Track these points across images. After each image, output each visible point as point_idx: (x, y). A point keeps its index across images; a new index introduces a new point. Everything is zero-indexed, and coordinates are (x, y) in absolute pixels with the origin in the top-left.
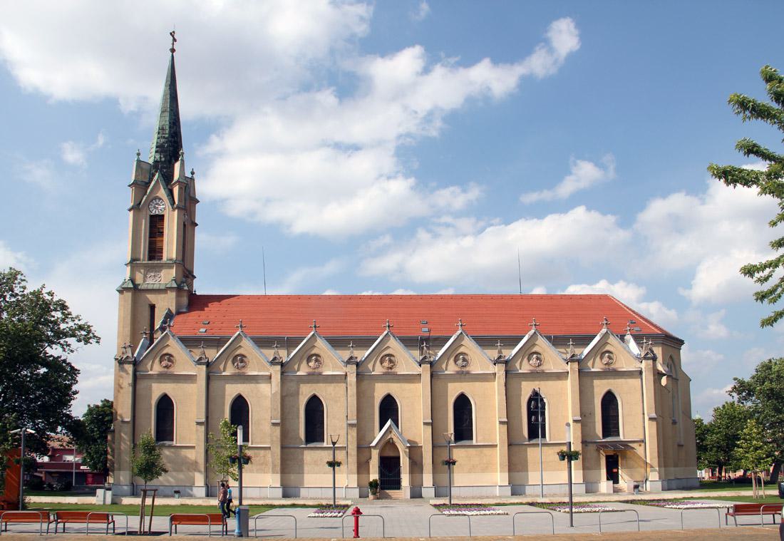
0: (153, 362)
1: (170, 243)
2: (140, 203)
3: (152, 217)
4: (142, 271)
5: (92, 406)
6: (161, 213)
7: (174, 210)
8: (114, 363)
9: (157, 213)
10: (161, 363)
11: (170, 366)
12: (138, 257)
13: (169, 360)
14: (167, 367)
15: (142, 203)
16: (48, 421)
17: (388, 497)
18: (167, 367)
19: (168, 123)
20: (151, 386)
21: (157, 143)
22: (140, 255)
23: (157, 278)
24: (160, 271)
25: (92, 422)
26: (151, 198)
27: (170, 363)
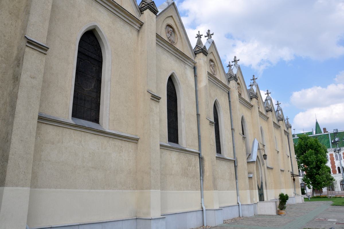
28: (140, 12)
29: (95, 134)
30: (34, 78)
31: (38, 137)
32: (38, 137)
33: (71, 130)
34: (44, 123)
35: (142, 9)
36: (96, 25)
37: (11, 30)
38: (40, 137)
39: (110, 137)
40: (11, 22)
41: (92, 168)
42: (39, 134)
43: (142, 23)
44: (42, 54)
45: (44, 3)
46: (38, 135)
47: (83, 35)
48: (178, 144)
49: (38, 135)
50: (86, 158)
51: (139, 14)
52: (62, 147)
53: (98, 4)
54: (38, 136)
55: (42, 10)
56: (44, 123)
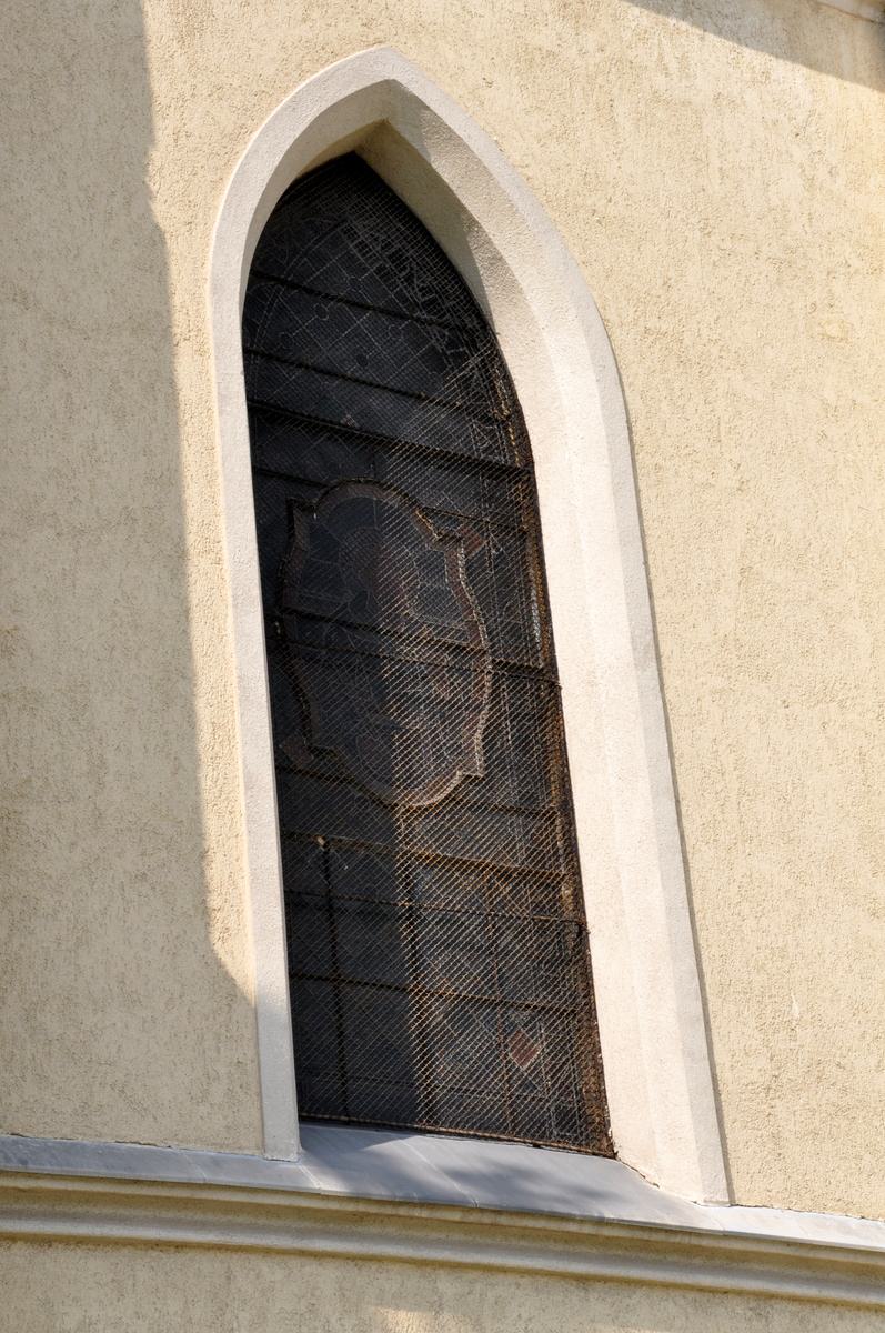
29: (583, 1280)
36: (390, 88)
39: (758, 1295)
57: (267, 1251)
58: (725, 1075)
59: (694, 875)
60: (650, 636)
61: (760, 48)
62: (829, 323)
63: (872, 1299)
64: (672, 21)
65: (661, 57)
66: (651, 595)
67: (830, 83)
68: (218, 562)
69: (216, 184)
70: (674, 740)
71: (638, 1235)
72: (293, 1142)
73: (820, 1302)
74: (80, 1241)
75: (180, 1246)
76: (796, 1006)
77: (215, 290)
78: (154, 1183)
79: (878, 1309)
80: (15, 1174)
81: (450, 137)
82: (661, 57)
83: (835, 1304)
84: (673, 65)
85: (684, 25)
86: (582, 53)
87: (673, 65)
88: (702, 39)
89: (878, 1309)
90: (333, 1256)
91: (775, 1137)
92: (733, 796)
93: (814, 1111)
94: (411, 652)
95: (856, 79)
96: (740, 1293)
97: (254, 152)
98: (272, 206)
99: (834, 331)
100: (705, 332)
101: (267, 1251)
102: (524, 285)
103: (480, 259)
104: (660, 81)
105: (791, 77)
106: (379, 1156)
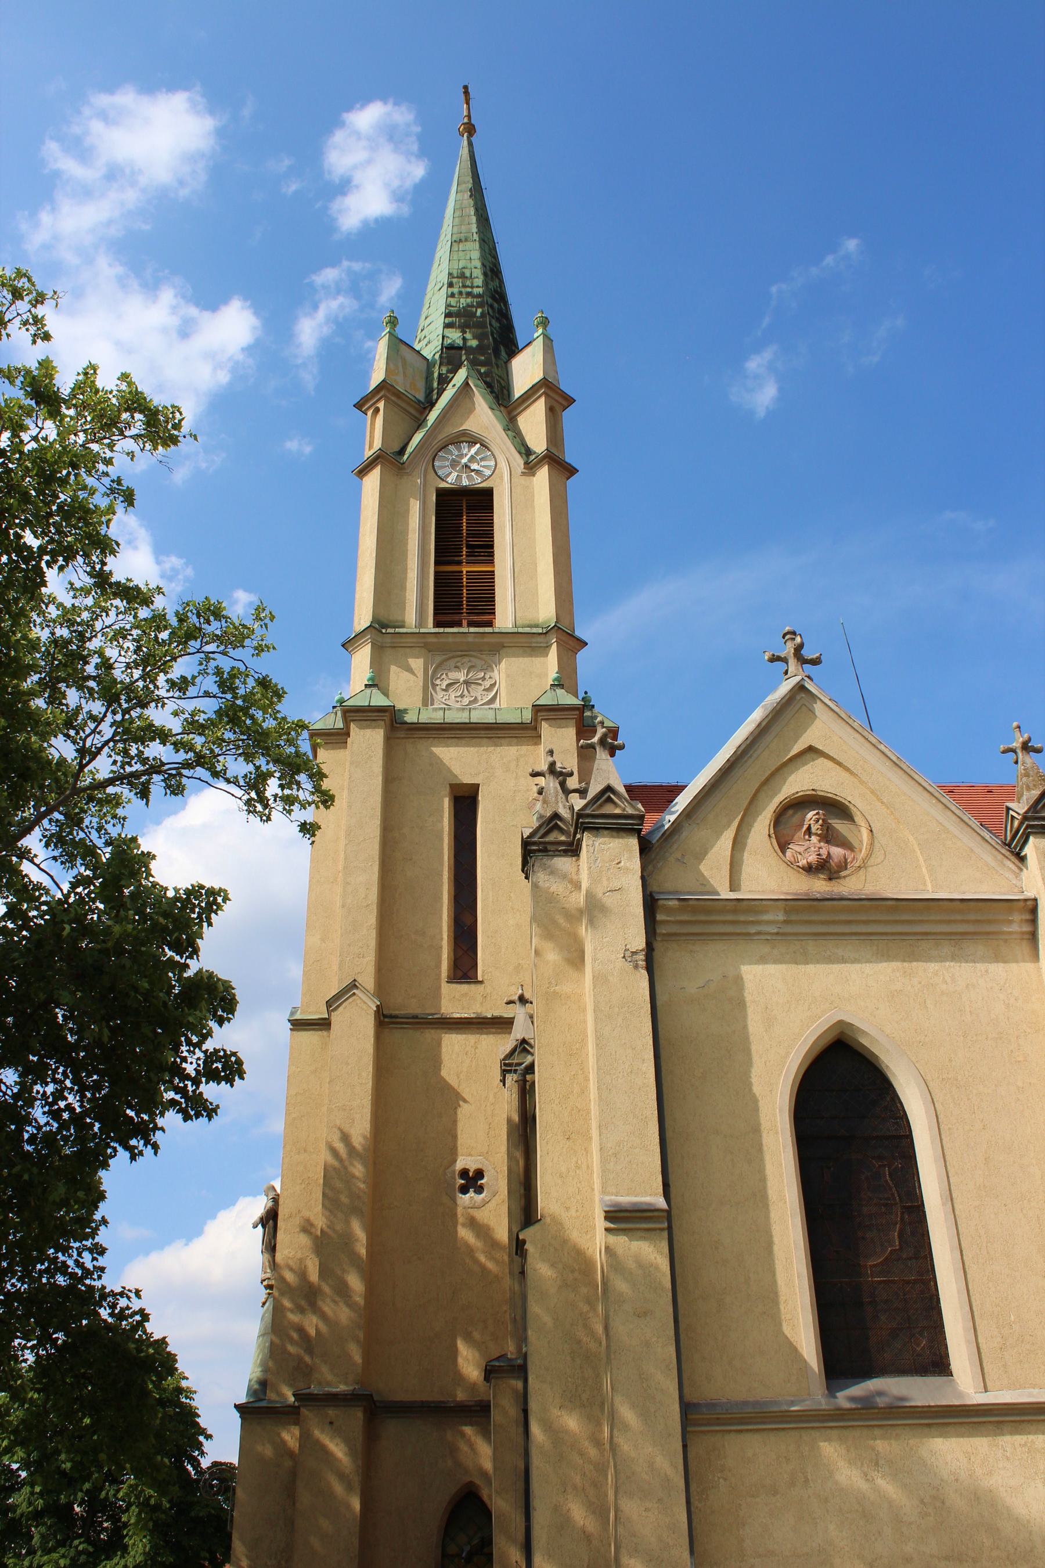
0: (738, 843)
1: (523, 573)
2: (402, 451)
3: (441, 493)
4: (417, 664)
5: (180, 796)
6: (478, 482)
7: (530, 468)
8: (109, 1220)
9: (465, 482)
10: (783, 847)
11: (843, 865)
12: (395, 616)
13: (829, 836)
14: (822, 868)
15: (410, 449)
16: (63, 1146)
17: (610, 1206)
18: (822, 868)
19: (478, 264)
20: (738, 980)
21: (448, 306)
22: (402, 605)
23: (477, 691)
24: (488, 668)
25: (189, 628)
26: (436, 443)
27: (837, 852)
28: (1013, 858)
29: (929, 1425)
30: (645, 1314)
31: (721, 1480)
32: (721, 1480)
33: (829, 1431)
34: (730, 1431)
35: (1016, 845)
36: (841, 1023)
37: (579, 1185)
38: (725, 1479)
39: (998, 1422)
40: (575, 1159)
41: (947, 1558)
42: (722, 1471)
43: (1029, 903)
44: (654, 1232)
45: (631, 1072)
46: (719, 1475)
47: (802, 1080)
48: (236, 1406)
49: (719, 1475)
50: (910, 1523)
51: (1011, 866)
52: (809, 1497)
53: (828, 938)
54: (719, 1478)
55: (629, 1097)
56: (730, 1431)
57: (813, 1428)
58: (983, 1346)
59: (969, 1276)
60: (948, 1192)
61: (983, 962)
62: (1018, 1056)
63: (1042, 1418)
64: (947, 964)
65: (944, 978)
66: (948, 1177)
67: (1014, 966)
68: (785, 1202)
69: (779, 1075)
70: (960, 1229)
71: (948, 1409)
72: (502, 702)
73: (1023, 1421)
74: (751, 1430)
75: (783, 1429)
76: (1012, 1317)
77: (780, 1111)
78: (770, 1412)
79: (1043, 1421)
80: (725, 1414)
81: (863, 1032)
82: (944, 978)
83: (1029, 1421)
84: (949, 980)
85: (952, 964)
86: (913, 986)
87: (949, 980)
88: (960, 966)
89: (1043, 1421)
90: (836, 1427)
91: (1005, 1366)
92: (984, 1244)
93: (1020, 1354)
94: (651, 1250)
95: (1024, 961)
96: (990, 1422)
97: (792, 1060)
98: (800, 1077)
99: (1021, 1059)
100: (966, 1073)
101: (813, 1428)
102: (896, 1073)
103: (883, 1066)
104: (944, 987)
105: (997, 969)
106: (432, 753)
